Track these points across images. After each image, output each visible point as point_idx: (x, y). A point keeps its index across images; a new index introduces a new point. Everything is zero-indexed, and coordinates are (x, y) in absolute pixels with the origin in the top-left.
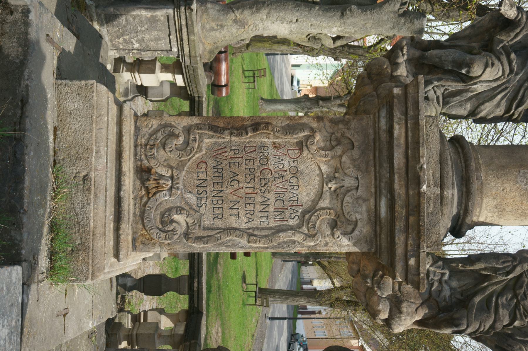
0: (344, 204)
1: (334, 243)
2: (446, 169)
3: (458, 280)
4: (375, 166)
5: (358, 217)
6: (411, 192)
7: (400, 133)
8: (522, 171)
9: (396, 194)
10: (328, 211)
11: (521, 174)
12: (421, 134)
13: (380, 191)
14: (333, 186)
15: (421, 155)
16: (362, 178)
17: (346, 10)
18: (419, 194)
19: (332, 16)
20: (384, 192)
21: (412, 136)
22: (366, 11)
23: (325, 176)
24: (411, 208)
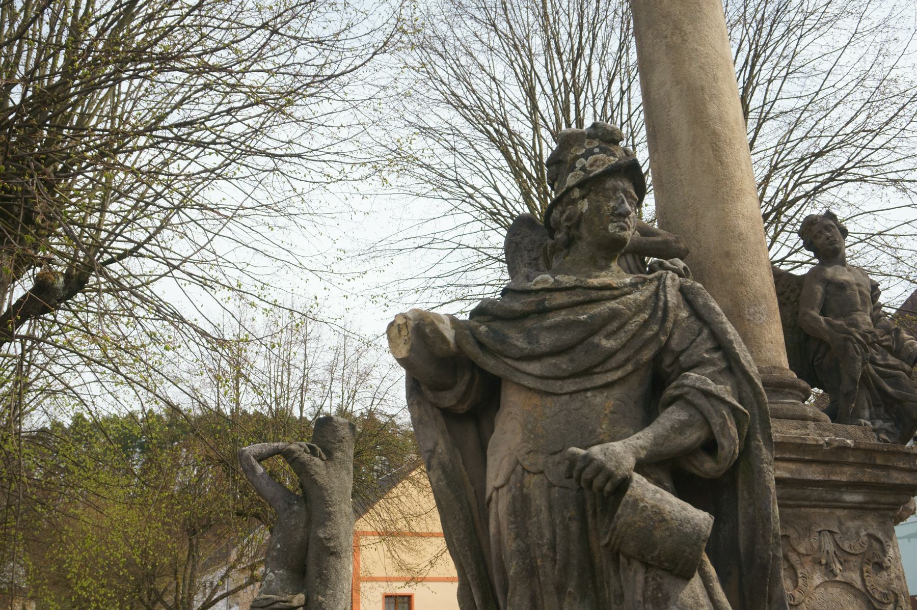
0: (853, 552)
1: (896, 567)
2: (785, 411)
3: (863, 408)
4: (800, 506)
5: (863, 533)
6: (851, 459)
7: (785, 469)
8: (748, 317)
9: (851, 479)
10: (866, 574)
11: (751, 318)
12: (792, 441)
13: (835, 501)
14: (837, 567)
15: (814, 443)
16: (820, 526)
17: (329, 548)
18: (856, 449)
19: (336, 571)
20: (837, 495)
21: (790, 452)
22: (330, 514)
23: (827, 579)
24: (867, 461)
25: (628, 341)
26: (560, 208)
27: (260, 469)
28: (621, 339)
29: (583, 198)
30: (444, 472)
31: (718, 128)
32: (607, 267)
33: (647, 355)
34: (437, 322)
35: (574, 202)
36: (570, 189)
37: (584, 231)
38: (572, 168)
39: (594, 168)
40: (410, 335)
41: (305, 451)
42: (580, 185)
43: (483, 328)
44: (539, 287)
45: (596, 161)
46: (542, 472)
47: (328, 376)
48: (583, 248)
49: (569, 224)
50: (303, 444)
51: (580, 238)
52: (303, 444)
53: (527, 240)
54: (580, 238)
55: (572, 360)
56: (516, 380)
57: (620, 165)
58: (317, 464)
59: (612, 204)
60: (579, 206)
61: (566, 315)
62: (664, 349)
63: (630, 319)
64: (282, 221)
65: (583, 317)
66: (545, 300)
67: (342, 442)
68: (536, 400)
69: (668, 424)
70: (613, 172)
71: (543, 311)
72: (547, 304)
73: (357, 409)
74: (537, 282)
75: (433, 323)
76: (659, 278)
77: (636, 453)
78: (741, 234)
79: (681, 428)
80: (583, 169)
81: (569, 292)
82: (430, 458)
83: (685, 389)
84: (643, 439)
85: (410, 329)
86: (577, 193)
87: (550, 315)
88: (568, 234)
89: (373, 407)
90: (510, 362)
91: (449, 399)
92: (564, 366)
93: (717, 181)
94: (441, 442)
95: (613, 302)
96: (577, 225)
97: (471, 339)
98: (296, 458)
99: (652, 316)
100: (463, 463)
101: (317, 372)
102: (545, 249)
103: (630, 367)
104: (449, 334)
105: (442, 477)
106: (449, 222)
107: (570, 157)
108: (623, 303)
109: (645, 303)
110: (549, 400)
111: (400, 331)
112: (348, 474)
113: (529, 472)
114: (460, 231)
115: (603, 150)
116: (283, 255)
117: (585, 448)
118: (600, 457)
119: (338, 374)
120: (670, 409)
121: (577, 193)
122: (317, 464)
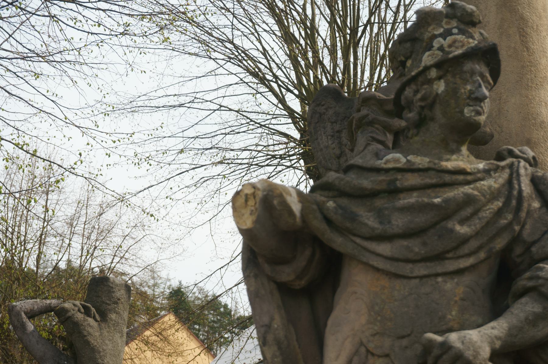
25: (482, 228)
26: (413, 87)
27: (30, 326)
28: (475, 225)
29: (439, 78)
30: (280, 348)
31: (527, 14)
32: (457, 151)
33: (500, 244)
34: (284, 195)
35: (430, 82)
36: (427, 69)
37: (438, 112)
38: (430, 47)
39: (453, 49)
40: (257, 205)
41: (79, 310)
42: (438, 65)
43: (331, 204)
44: (390, 165)
45: (455, 41)
46: (387, 356)
47: (67, 231)
48: (435, 129)
49: (423, 104)
50: (78, 303)
51: (432, 119)
52: (78, 303)
53: (331, 112)
54: (432, 119)
55: (424, 244)
56: (365, 260)
57: (480, 48)
58: (91, 324)
59: (469, 87)
60: (435, 87)
61: (418, 197)
62: (516, 239)
63: (484, 205)
64: (45, 68)
65: (437, 200)
66: (396, 179)
67: (117, 303)
68: (384, 281)
69: (522, 315)
70: (471, 54)
71: (394, 192)
72: (398, 184)
73: (95, 265)
74: (387, 162)
75: (281, 196)
76: (511, 166)
77: (491, 343)
78: (543, 122)
79: (534, 320)
80: (441, 48)
81: (421, 173)
82: (266, 333)
83: (540, 281)
84: (497, 328)
85: (258, 200)
86: (433, 73)
87: (402, 196)
88: (420, 114)
89: (113, 265)
90: (358, 240)
91: (287, 274)
92: (417, 250)
93: (523, 67)
94: (277, 318)
95: (466, 187)
96: (431, 106)
97: (318, 215)
98: (69, 317)
99: (507, 203)
100: (297, 340)
101: (57, 224)
102: (351, 123)
103: (482, 255)
104: (296, 207)
105: (278, 354)
106: (209, 83)
107: (427, 36)
108: (476, 189)
109: (499, 191)
110: (398, 283)
111: (246, 201)
112: (122, 336)
113: (373, 354)
114: (221, 92)
115: (462, 32)
116: (48, 106)
117: (441, 333)
118: (458, 345)
119: (79, 229)
120: (524, 300)
121: (433, 73)
122: (91, 324)
